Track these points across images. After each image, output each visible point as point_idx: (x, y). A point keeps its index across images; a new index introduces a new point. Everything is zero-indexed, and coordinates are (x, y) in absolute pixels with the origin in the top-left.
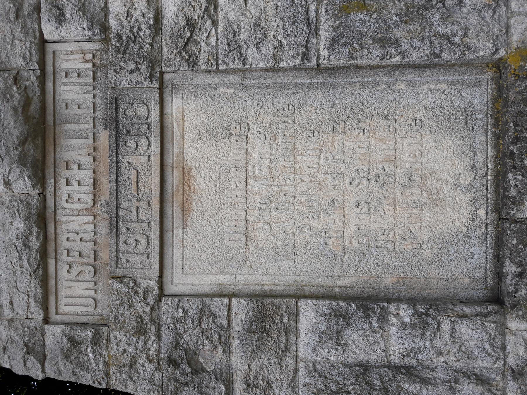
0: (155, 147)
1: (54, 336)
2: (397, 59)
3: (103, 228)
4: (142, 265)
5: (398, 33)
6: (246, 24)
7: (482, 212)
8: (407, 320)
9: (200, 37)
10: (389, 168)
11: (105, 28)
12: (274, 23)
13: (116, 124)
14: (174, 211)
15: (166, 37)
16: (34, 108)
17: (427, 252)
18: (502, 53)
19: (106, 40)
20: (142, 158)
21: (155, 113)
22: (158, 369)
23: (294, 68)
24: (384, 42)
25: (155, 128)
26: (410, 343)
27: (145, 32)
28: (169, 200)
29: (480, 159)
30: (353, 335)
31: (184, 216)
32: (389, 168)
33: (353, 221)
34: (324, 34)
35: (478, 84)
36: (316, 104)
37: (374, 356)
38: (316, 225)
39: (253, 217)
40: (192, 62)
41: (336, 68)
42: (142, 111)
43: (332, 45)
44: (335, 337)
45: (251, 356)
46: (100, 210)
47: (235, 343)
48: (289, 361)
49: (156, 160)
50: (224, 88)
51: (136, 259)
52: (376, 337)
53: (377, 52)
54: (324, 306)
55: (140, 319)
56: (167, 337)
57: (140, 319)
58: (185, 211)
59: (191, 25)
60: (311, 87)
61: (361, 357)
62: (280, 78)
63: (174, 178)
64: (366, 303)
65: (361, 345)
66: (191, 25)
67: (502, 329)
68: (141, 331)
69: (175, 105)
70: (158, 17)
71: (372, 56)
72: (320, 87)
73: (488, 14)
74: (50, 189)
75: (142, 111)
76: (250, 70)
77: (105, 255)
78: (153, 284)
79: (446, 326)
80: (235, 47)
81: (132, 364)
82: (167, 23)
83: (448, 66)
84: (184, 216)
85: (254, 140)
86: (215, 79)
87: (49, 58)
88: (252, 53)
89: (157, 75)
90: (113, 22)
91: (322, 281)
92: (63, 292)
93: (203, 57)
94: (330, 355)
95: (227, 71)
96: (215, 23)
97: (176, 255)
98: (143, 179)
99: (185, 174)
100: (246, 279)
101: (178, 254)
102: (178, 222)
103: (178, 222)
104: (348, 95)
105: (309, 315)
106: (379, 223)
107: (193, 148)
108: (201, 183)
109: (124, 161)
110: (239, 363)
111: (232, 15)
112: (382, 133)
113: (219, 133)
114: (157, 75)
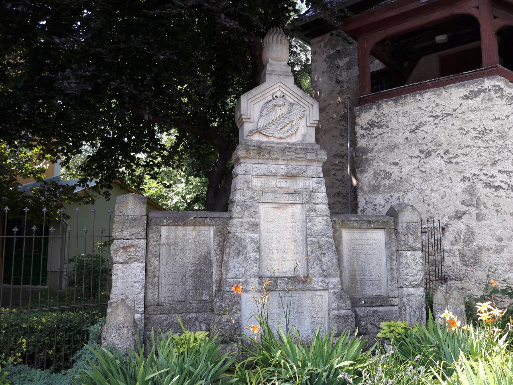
0: (290, 202)
1: (249, 177)
2: (309, 254)
3: (272, 189)
4: (266, 198)
5: (314, 254)
6: (316, 223)
7: (277, 274)
8: (413, 179)
9: (313, 213)
10: (286, 254)
11: (315, 192)
12: (316, 229)
13: (295, 193)
14: (277, 205)
15: (313, 205)
16: (299, 175)
17: (269, 262)
18: (310, 276)
19: (312, 192)
20: (288, 199)
21: (297, 202)
22: (243, 202)
23: (307, 233)
24: (312, 251)
25: (294, 202)
26: (252, 257)
27: (314, 201)
28: (279, 205)
29: (289, 273)
30: (253, 245)
31: (275, 208)
32: (286, 254)
33: (275, 246)
34: (314, 239)
35: (304, 272)
36: (300, 238)
37: (249, 250)
38: (274, 238)
39: (275, 223)
40: (308, 211)
41: (307, 242)
42: (298, 199)
43: (312, 241)
44: (253, 241)
45: (247, 223)
46: (276, 189)
47: (250, 219)
48: (246, 231)
49: (288, 202)
50: (303, 218)
51: (266, 197)
52: (252, 250)
53: (310, 250)
54: (258, 239)
55: (255, 198)
56: (250, 204)
57: (255, 198)
58: (277, 208)
59: (315, 211)
60: (303, 237)
61: (248, 247)
62: (305, 230)
63: (284, 206)
64: (258, 250)
65: (250, 247)
66: (315, 211)
67: (255, 278)
68: (252, 198)
69: (299, 207)
70: (317, 204)
71: (309, 249)
72: (303, 239)
73: (318, 272)
74: (281, 177)
75: (298, 199)
76: (306, 223)
77: (266, 189)
78: (261, 201)
79: (256, 265)
80: (311, 220)
81: (244, 196)
82: (316, 206)
83: (308, 265)
84: (275, 208)
85: (292, 224)
86: (304, 216)
87: (308, 178)
88: (310, 224)
89: (305, 203)
90: (316, 194)
91: (262, 239)
92: (258, 179)
93: (309, 213)
94: (249, 240)
95: (306, 218)
96: (316, 216)
97: (267, 206)
98: (284, 199)
99: (284, 208)
100: (262, 222)
101: (267, 206)
102: (274, 206)
103: (274, 206)
104: (301, 244)
105: (256, 236)
106: (275, 251)
107: (290, 210)
108: (283, 212)
109: (287, 195)
110: (245, 220)
111: (317, 220)
112: (294, 252)
113: (293, 216)
114: (305, 203)
